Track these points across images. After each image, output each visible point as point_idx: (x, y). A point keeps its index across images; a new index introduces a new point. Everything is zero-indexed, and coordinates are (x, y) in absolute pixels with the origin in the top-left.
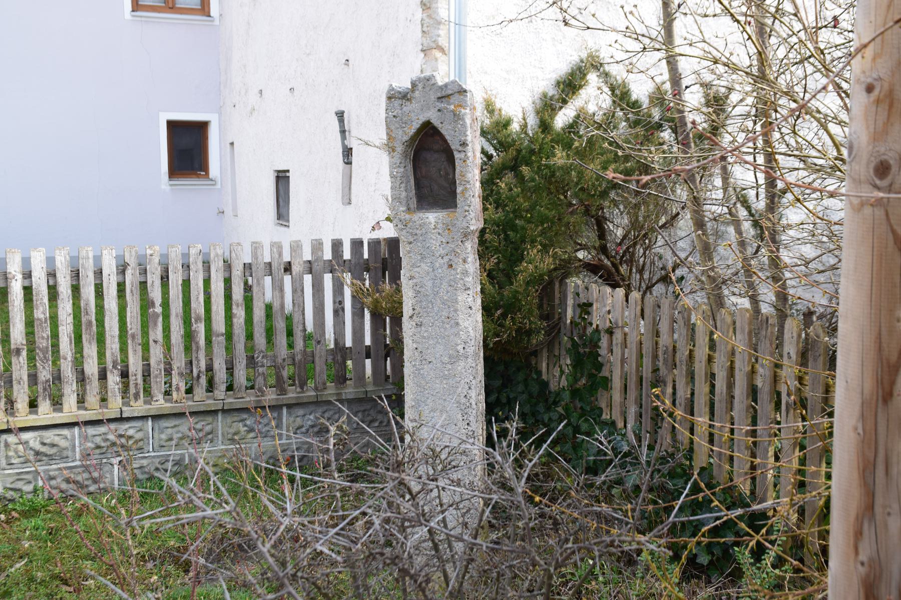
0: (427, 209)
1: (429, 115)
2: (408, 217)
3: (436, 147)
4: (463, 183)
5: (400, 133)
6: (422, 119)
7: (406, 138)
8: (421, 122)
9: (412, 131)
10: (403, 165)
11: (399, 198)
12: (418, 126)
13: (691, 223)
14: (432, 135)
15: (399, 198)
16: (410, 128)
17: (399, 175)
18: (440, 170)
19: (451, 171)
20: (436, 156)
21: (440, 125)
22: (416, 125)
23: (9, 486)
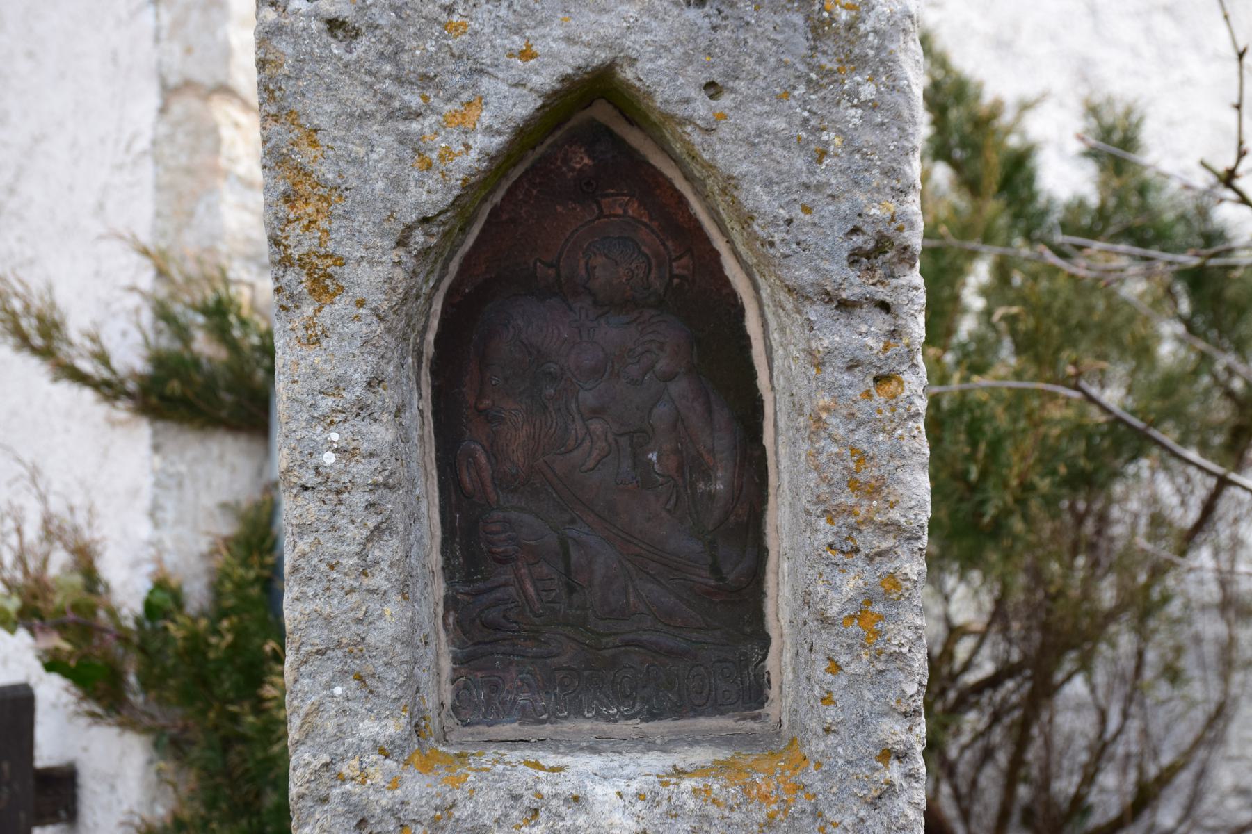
0: (529, 716)
1: (610, 25)
2: (419, 789)
3: (607, 271)
4: (871, 541)
5: (383, 149)
6: (560, 55)
7: (426, 195)
8: (545, 79)
9: (473, 146)
10: (388, 397)
11: (357, 648)
12: (524, 107)
13: (242, 577)
14: (588, 189)
15: (357, 648)
16: (461, 123)
17: (363, 470)
18: (639, 437)
19: (718, 445)
20: (612, 333)
21: (702, 107)
22: (508, 103)
23: (177, 308)
